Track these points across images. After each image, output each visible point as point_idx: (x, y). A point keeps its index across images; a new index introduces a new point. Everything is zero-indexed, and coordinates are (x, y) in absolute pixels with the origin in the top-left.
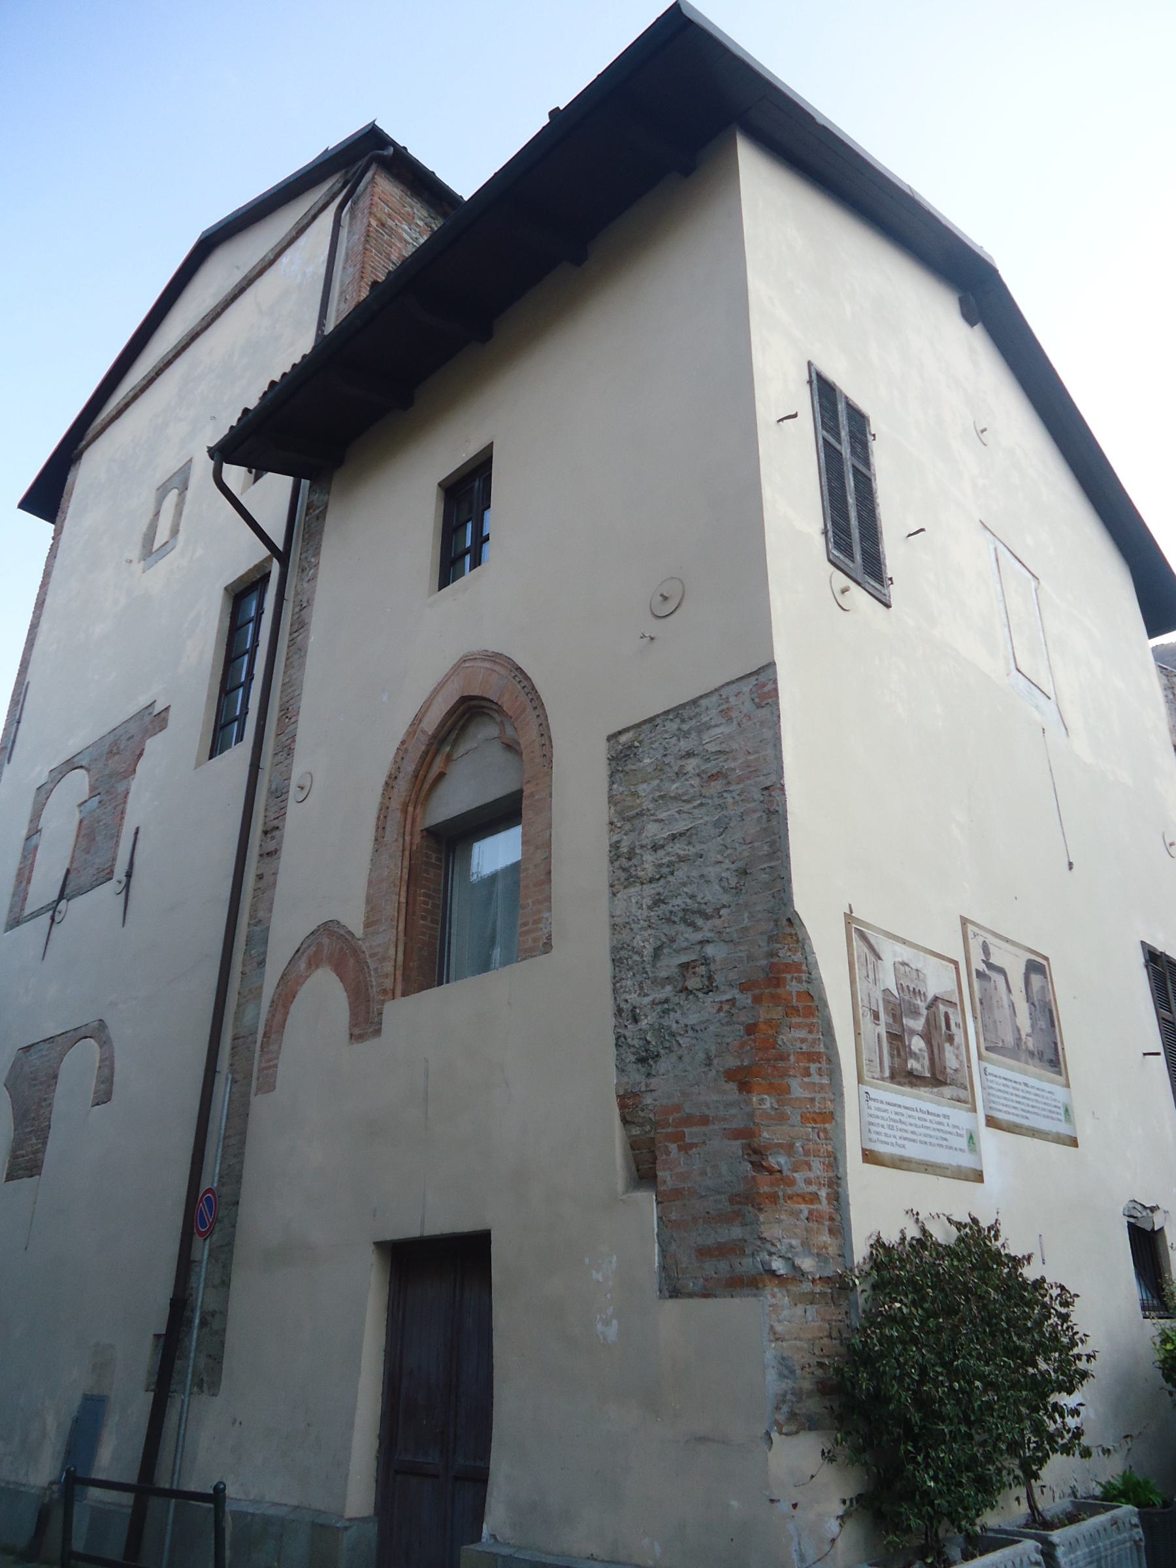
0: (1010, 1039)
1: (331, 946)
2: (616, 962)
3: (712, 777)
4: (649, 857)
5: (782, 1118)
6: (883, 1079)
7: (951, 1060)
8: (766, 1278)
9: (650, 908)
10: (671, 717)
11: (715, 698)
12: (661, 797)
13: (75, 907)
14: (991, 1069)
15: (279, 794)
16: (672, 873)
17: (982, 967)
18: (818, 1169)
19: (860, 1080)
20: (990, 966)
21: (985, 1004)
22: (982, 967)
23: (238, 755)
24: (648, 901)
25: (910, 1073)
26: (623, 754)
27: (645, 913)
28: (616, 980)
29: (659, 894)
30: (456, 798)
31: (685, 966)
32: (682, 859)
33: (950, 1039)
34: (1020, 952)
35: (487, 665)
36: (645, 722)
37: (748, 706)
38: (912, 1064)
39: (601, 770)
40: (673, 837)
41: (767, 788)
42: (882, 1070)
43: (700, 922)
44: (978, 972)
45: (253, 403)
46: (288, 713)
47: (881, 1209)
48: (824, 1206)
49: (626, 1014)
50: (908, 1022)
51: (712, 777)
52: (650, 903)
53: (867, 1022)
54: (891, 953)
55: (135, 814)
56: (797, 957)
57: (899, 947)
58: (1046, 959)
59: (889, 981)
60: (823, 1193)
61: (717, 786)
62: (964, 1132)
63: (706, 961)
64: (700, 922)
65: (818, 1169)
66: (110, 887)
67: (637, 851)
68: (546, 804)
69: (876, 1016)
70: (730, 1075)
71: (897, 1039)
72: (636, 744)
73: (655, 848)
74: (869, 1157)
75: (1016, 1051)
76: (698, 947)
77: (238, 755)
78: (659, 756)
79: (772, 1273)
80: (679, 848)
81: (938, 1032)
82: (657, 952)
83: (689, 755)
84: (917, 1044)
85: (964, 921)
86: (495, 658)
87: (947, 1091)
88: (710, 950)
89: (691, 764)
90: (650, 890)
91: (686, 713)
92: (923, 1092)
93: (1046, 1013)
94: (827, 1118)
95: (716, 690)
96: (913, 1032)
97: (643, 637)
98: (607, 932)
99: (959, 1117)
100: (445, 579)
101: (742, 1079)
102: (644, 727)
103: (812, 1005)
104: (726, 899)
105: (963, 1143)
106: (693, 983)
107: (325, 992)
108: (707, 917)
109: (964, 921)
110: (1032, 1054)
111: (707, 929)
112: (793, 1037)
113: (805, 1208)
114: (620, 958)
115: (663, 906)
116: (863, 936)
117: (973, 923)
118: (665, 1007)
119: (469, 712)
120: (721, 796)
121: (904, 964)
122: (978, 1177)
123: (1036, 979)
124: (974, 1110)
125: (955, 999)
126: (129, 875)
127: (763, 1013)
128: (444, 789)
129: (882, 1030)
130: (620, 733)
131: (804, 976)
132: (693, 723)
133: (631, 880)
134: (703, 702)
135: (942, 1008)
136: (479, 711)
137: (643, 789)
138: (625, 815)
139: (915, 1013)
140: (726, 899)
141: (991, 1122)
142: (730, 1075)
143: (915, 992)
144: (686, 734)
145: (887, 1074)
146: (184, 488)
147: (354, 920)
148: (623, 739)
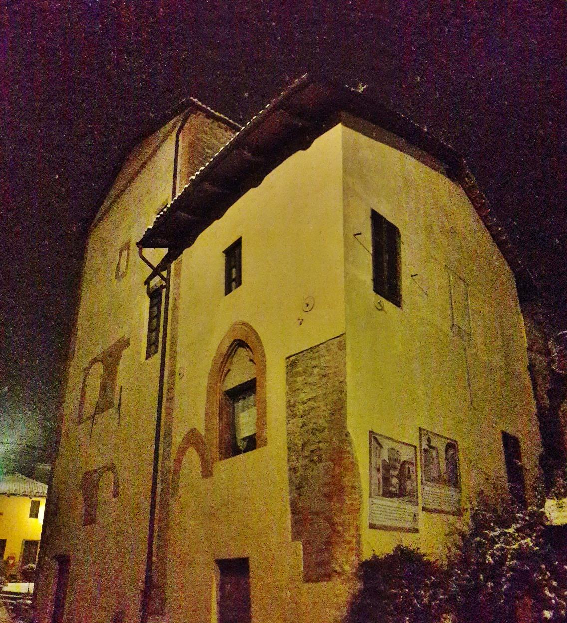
0: (436, 475)
1: (193, 439)
2: (289, 449)
3: (325, 376)
4: (301, 407)
5: (341, 511)
6: (379, 496)
7: (409, 486)
8: (334, 574)
9: (302, 428)
10: (309, 351)
11: (325, 345)
12: (306, 383)
13: (100, 419)
14: (427, 488)
15: (172, 375)
16: (309, 414)
17: (427, 447)
18: (353, 531)
19: (370, 496)
20: (431, 447)
21: (427, 463)
22: (427, 447)
23: (157, 357)
24: (301, 425)
25: (391, 492)
26: (292, 364)
27: (299, 429)
28: (289, 456)
29: (304, 422)
30: (234, 380)
31: (312, 451)
32: (313, 408)
33: (409, 478)
34: (443, 440)
35: (240, 326)
36: (300, 353)
37: (337, 350)
38: (393, 489)
39: (283, 370)
40: (310, 400)
41: (341, 382)
42: (379, 492)
43: (317, 434)
44: (424, 449)
45: (300, 152)
46: (174, 344)
47: (378, 545)
48: (354, 544)
49: (293, 470)
50: (393, 472)
51: (325, 376)
52: (301, 425)
53: (374, 472)
54: (387, 444)
55: (121, 381)
56: (349, 449)
57: (391, 442)
58: (455, 441)
59: (385, 455)
60: (354, 540)
61: (324, 380)
62: (412, 514)
63: (320, 450)
64: (317, 434)
65: (353, 531)
66: (112, 411)
67: (297, 404)
68: (263, 387)
69: (378, 470)
70: (325, 495)
71: (386, 480)
72: (296, 362)
73: (304, 403)
74: (372, 526)
75: (439, 480)
76: (318, 444)
77: (157, 357)
78: (305, 367)
79: (336, 571)
80: (312, 404)
81: (404, 476)
82: (304, 446)
83: (315, 367)
84: (395, 481)
85: (420, 429)
86: (244, 324)
87: (406, 498)
88: (321, 445)
89: (316, 371)
90: (301, 420)
91: (315, 350)
92: (395, 499)
93: (453, 464)
94: (356, 511)
95: (326, 342)
96: (393, 476)
97: (299, 320)
98: (285, 435)
99: (410, 508)
100: (228, 290)
101: (329, 496)
102: (300, 355)
103: (354, 465)
104: (327, 425)
105: (411, 518)
106: (316, 458)
107: (192, 457)
108: (321, 432)
109: (420, 429)
110: (445, 480)
111: (321, 436)
112: (346, 481)
113: (348, 546)
114: (291, 448)
115: (306, 427)
116: (376, 439)
117: (424, 430)
118: (306, 468)
119: (240, 344)
120: (326, 383)
121: (392, 449)
122: (416, 531)
123: (451, 452)
124: (417, 504)
125: (413, 461)
126: (120, 405)
127: (337, 471)
128: (231, 374)
129: (380, 475)
130: (291, 357)
131: (351, 456)
132: (317, 354)
133: (295, 416)
134: (321, 346)
135: (407, 466)
136: (242, 343)
137: (300, 379)
138: (292, 389)
139: (395, 468)
140: (327, 425)
141: (424, 509)
142: (325, 495)
143: (396, 460)
144: (315, 359)
145: (381, 493)
146: (129, 248)
147: (201, 430)
148: (292, 359)
